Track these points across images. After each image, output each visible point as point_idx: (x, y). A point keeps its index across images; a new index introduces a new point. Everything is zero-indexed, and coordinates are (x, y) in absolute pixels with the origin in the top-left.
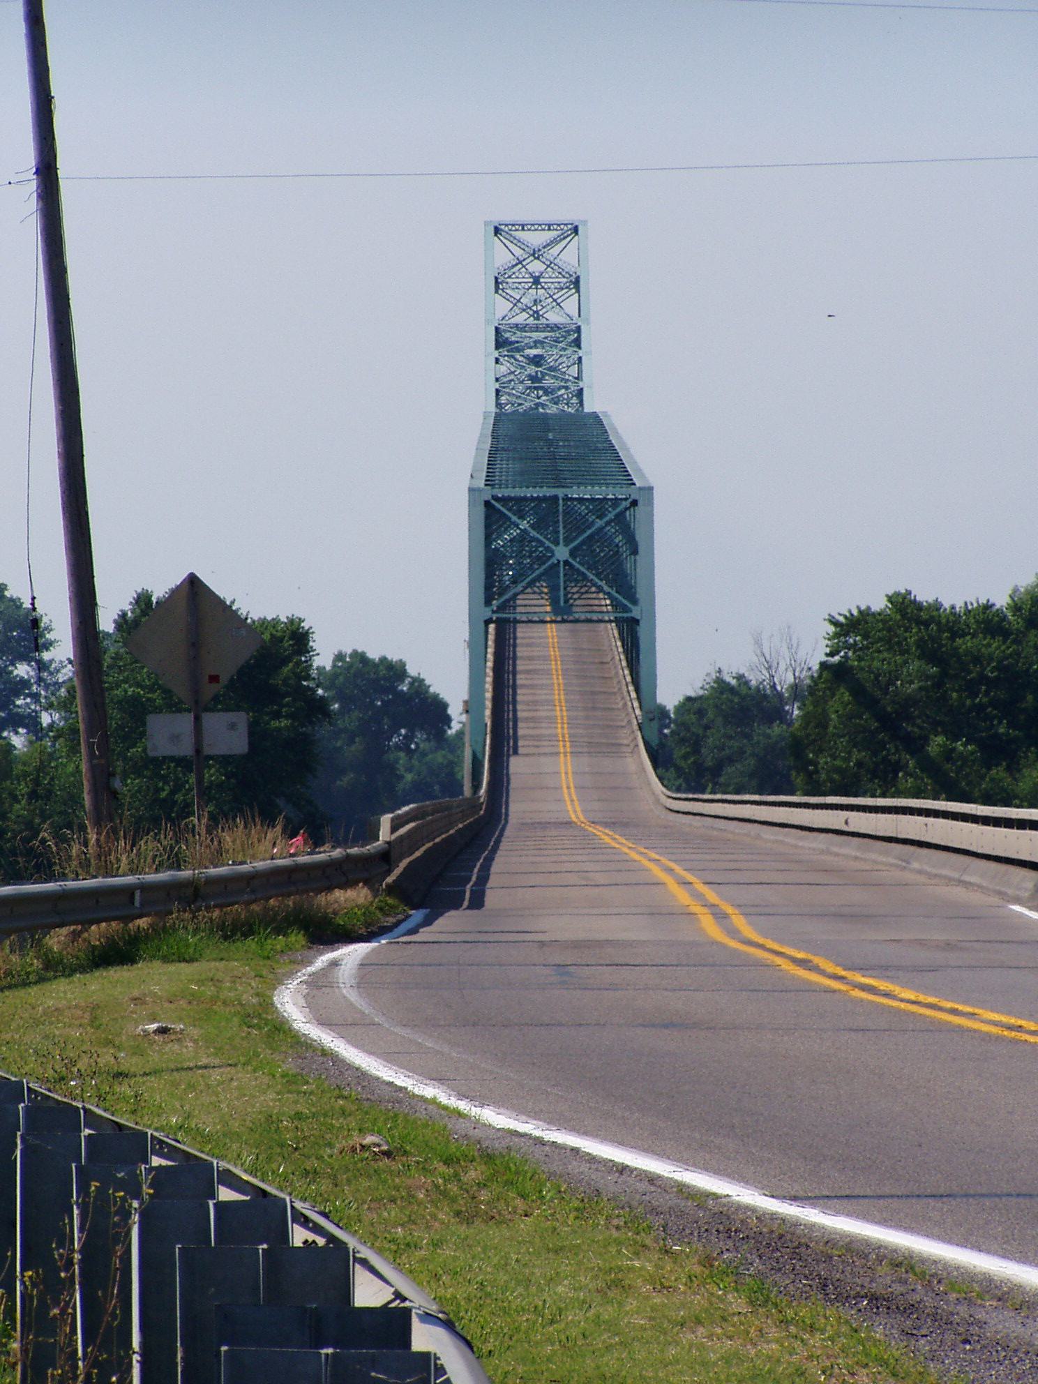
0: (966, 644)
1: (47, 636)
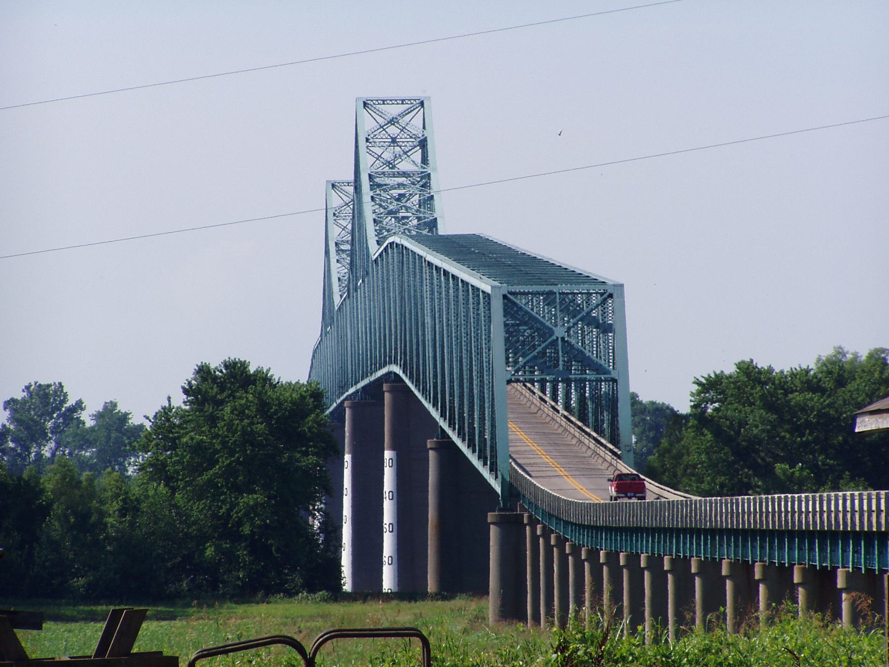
0: (797, 398)
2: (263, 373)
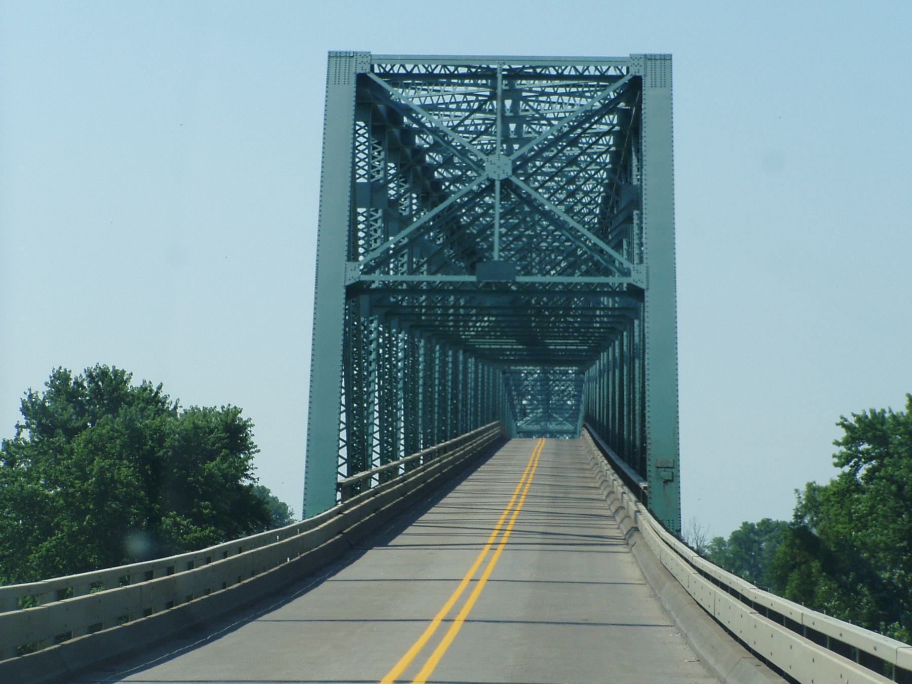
1: (291, 517)
2: (151, 391)
